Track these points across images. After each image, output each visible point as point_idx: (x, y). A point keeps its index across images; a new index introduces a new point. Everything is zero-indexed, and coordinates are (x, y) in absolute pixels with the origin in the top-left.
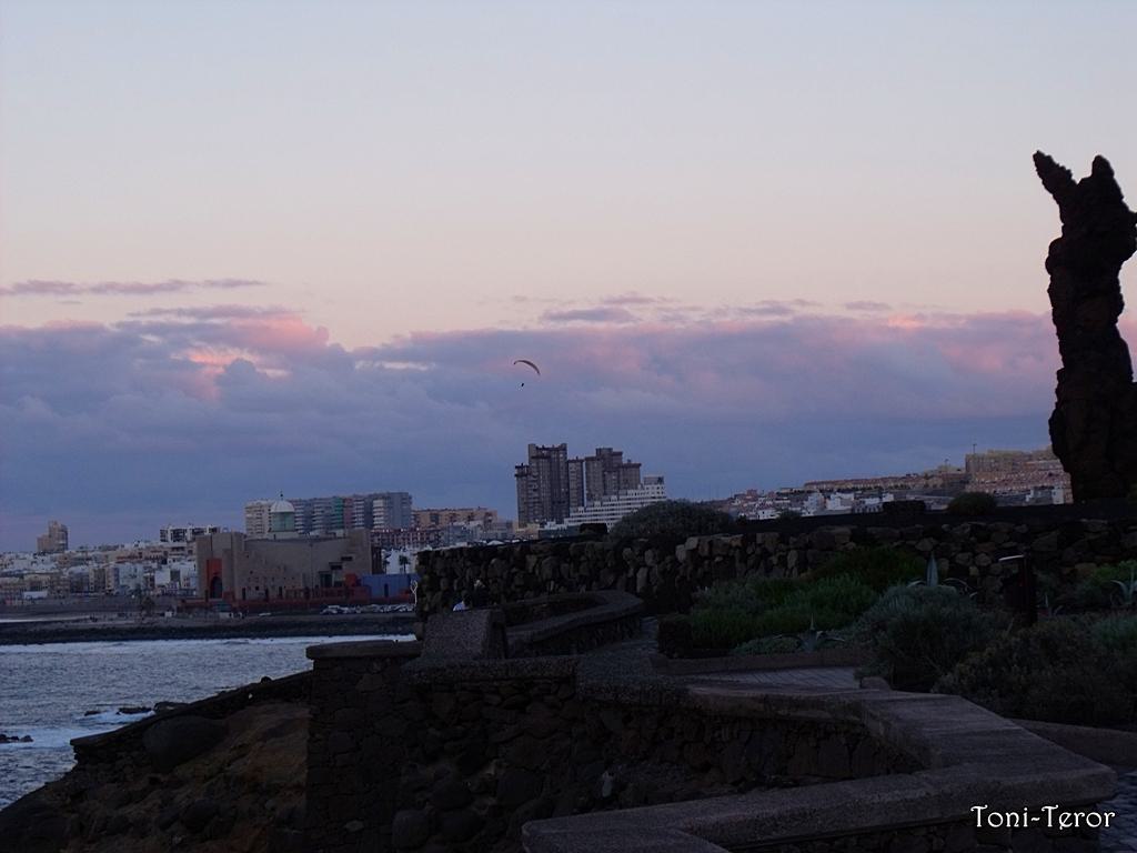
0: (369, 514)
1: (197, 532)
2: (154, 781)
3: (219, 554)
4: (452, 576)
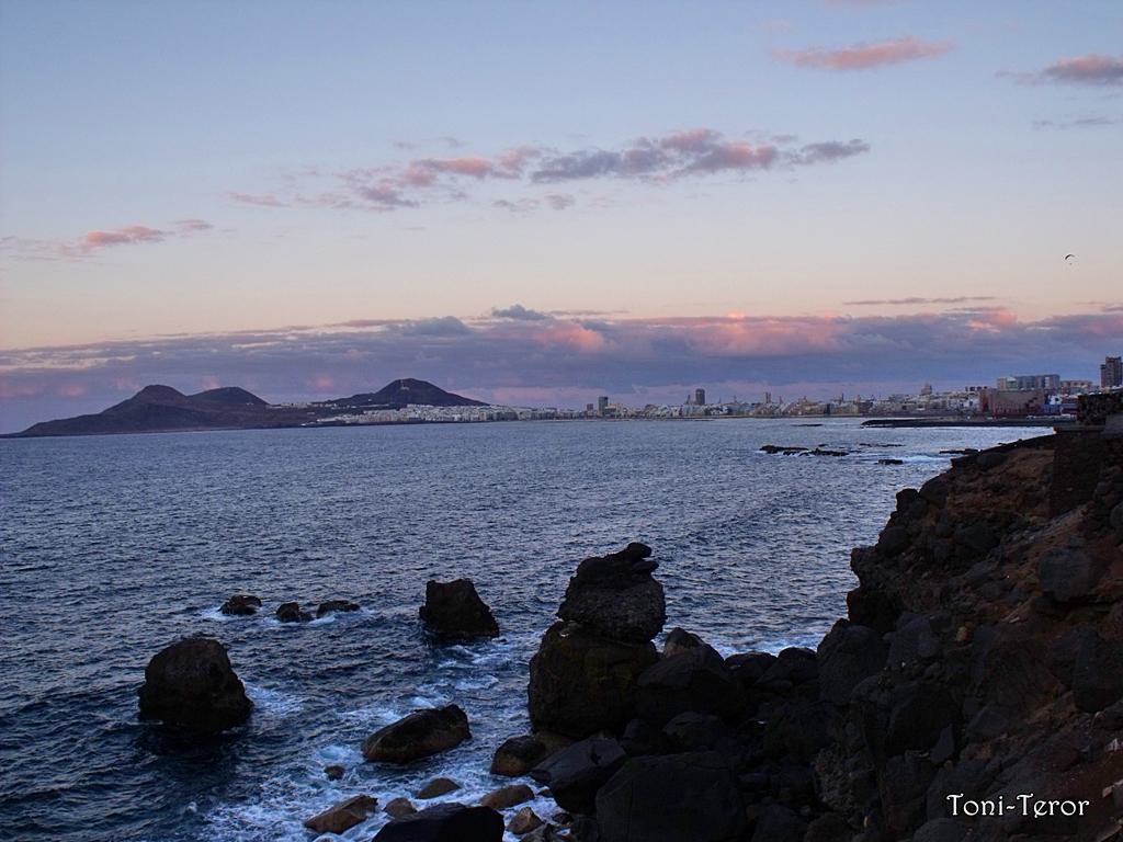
0: (1044, 382)
1: (979, 388)
2: (980, 475)
3: (987, 395)
4: (1091, 404)
